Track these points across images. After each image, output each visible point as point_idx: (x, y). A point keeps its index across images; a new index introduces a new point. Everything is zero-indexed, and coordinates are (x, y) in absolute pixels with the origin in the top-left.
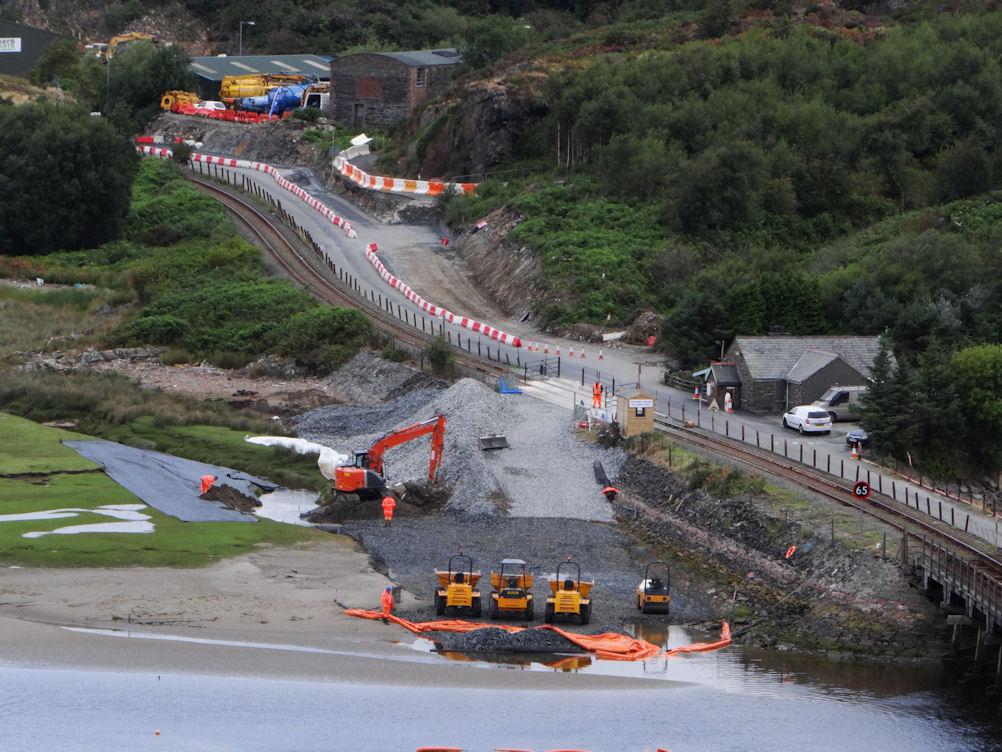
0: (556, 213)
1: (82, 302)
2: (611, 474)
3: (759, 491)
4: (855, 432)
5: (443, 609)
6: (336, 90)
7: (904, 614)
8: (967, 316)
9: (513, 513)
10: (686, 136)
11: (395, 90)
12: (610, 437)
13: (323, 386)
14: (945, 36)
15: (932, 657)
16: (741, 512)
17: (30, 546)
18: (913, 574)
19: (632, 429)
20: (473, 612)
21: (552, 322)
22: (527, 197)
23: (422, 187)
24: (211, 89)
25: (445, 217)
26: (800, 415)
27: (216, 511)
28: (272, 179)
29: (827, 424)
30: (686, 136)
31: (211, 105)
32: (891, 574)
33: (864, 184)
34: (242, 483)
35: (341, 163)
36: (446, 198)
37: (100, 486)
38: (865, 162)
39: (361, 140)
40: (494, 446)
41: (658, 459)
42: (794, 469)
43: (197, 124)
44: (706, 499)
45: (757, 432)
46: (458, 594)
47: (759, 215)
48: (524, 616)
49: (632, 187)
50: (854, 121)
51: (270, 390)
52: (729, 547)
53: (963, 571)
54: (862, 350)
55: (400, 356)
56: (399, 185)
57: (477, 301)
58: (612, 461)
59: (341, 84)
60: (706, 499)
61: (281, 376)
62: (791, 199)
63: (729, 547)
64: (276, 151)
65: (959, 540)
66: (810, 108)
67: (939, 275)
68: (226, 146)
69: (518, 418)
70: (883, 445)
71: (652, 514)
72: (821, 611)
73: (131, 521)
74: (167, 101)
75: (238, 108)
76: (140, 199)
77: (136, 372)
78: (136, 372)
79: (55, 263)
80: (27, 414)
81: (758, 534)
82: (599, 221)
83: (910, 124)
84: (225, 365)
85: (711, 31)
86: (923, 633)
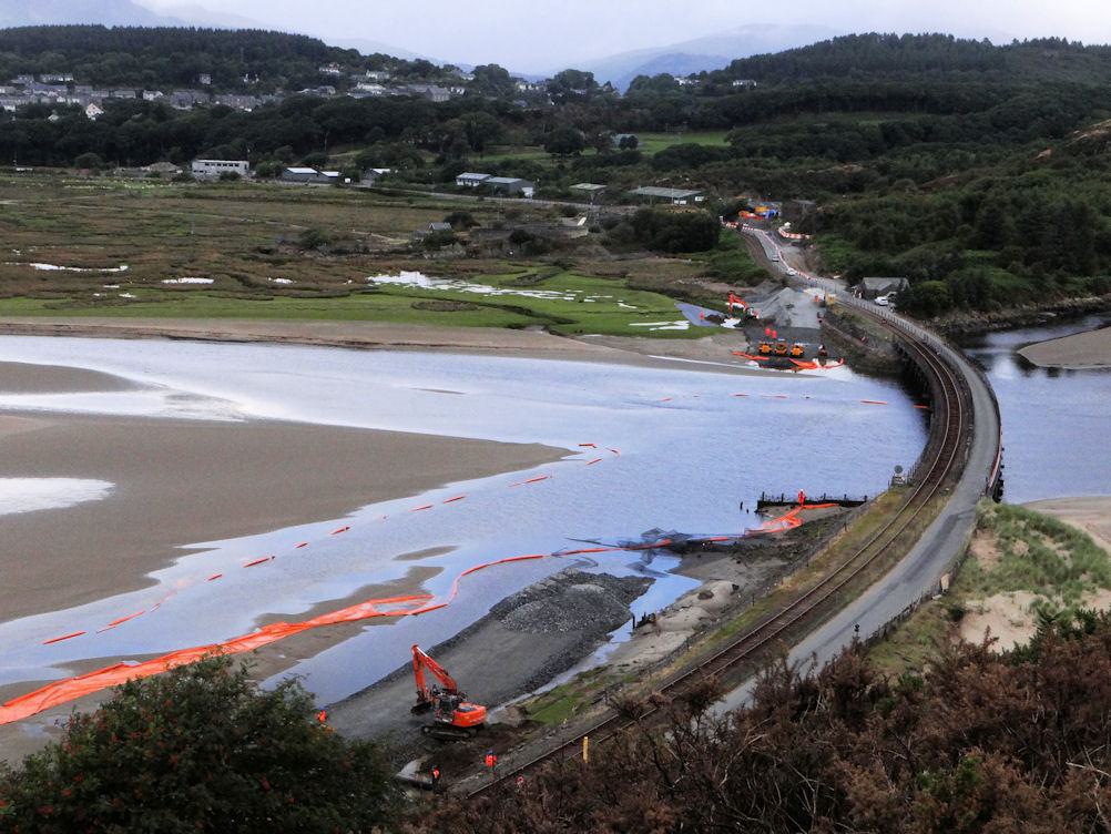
0: (828, 244)
1: (699, 265)
2: (822, 316)
3: (858, 321)
4: (893, 305)
5: (761, 353)
6: (783, 212)
7: (891, 357)
8: (930, 272)
9: (792, 325)
10: (867, 223)
11: (799, 211)
12: (823, 304)
13: (754, 289)
14: (944, 197)
15: (899, 370)
16: (854, 328)
17: (649, 332)
18: (896, 346)
19: (829, 303)
20: (769, 354)
21: (821, 273)
22: (822, 240)
23: (799, 236)
24: (752, 211)
25: (803, 245)
26: (879, 299)
27: (708, 323)
28: (761, 234)
29: (886, 303)
30: (867, 223)
31: (752, 215)
32: (889, 346)
33: (915, 236)
34: (721, 315)
35: (780, 230)
36: (804, 238)
37: (679, 316)
38: (916, 230)
39: (787, 224)
40: (790, 307)
41: (835, 311)
42: (873, 315)
43: (747, 220)
44: (845, 323)
45: (866, 304)
46: (766, 349)
47: (884, 244)
48: (785, 355)
49: (850, 236)
50: (915, 219)
51: (739, 290)
52: (848, 337)
53: (907, 344)
54: (896, 281)
55: (774, 281)
56: (793, 236)
57: (804, 267)
58: (822, 312)
59: (784, 209)
60: (845, 323)
61: (742, 286)
62: (893, 241)
63: (848, 337)
64: (765, 226)
65: (909, 335)
66: (903, 216)
67: (923, 261)
68: (753, 226)
69: (799, 299)
70: (899, 310)
71: (830, 327)
72: (868, 356)
73: (683, 325)
74: (740, 213)
75: (759, 216)
76: (722, 238)
77: (704, 284)
78: (704, 284)
79: (694, 255)
80: (669, 296)
81: (856, 334)
82: (840, 246)
83: (930, 220)
84: (728, 283)
85: (881, 195)
86: (899, 362)
